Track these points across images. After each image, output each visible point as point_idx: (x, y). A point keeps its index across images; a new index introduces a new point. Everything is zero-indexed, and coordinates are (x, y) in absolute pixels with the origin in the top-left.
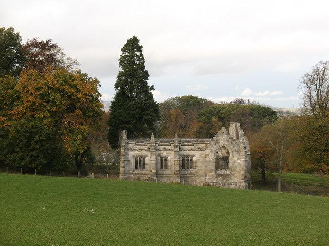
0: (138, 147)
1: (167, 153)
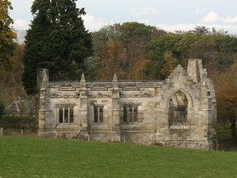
0: (63, 93)
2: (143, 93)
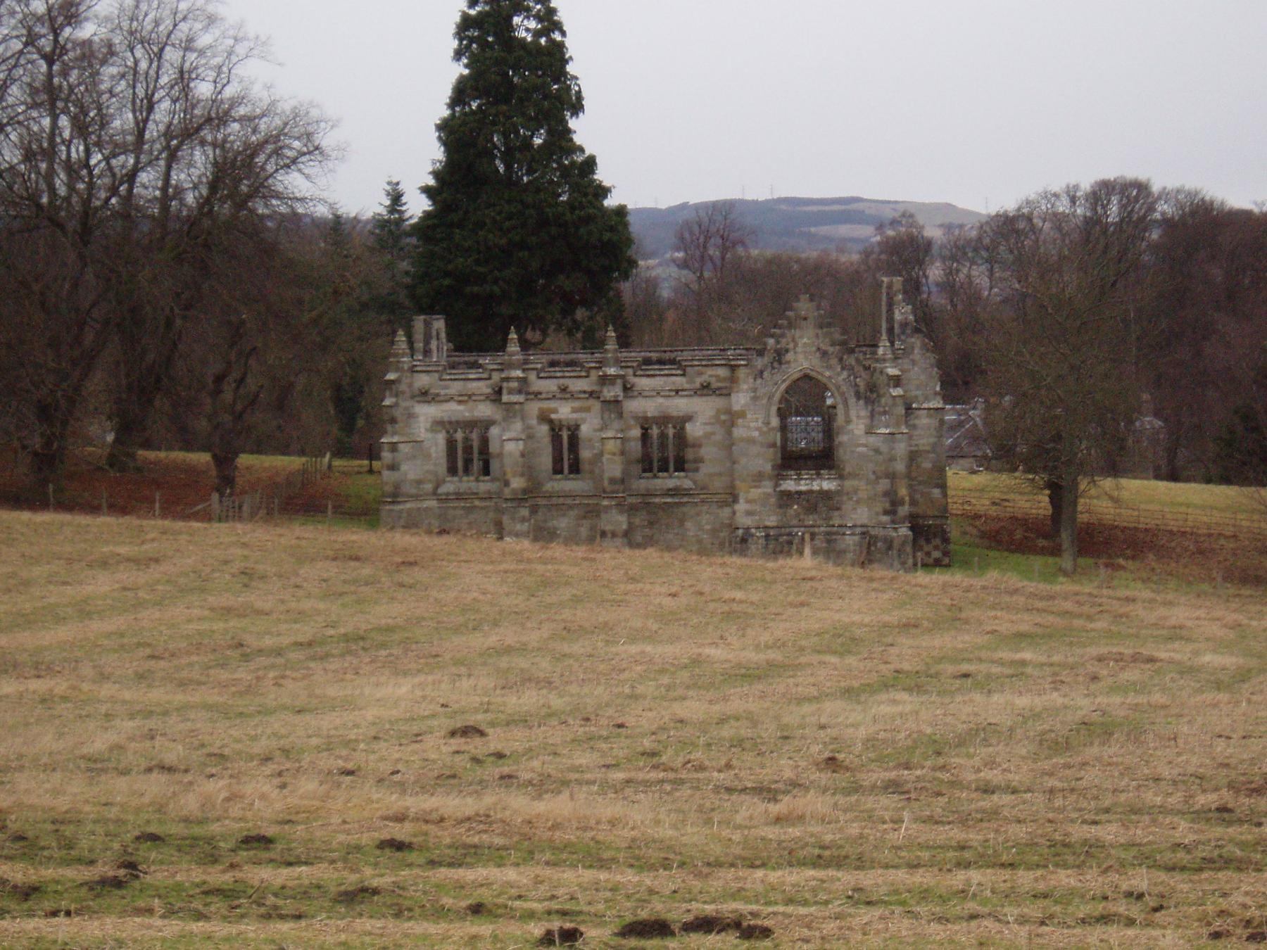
0: (455, 388)
1: (575, 410)
2: (697, 385)
